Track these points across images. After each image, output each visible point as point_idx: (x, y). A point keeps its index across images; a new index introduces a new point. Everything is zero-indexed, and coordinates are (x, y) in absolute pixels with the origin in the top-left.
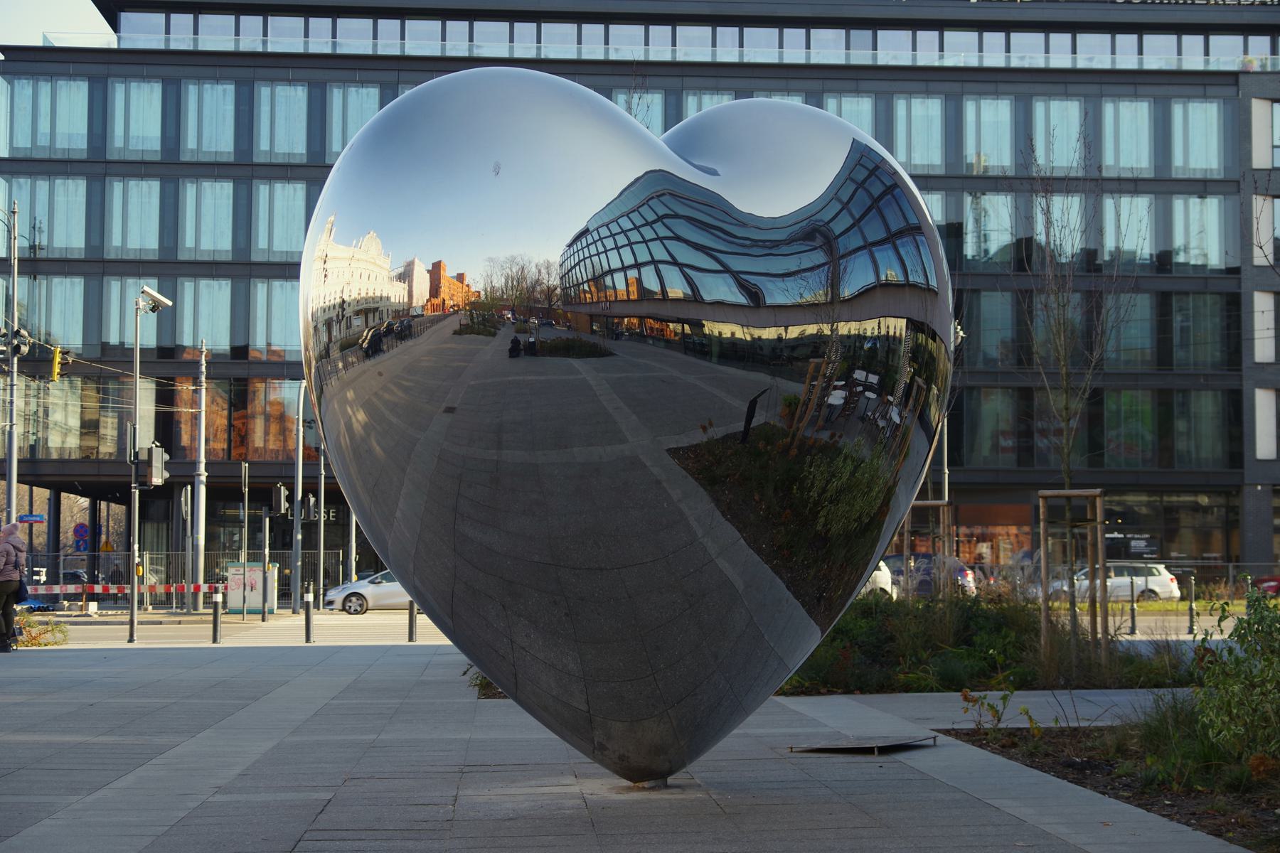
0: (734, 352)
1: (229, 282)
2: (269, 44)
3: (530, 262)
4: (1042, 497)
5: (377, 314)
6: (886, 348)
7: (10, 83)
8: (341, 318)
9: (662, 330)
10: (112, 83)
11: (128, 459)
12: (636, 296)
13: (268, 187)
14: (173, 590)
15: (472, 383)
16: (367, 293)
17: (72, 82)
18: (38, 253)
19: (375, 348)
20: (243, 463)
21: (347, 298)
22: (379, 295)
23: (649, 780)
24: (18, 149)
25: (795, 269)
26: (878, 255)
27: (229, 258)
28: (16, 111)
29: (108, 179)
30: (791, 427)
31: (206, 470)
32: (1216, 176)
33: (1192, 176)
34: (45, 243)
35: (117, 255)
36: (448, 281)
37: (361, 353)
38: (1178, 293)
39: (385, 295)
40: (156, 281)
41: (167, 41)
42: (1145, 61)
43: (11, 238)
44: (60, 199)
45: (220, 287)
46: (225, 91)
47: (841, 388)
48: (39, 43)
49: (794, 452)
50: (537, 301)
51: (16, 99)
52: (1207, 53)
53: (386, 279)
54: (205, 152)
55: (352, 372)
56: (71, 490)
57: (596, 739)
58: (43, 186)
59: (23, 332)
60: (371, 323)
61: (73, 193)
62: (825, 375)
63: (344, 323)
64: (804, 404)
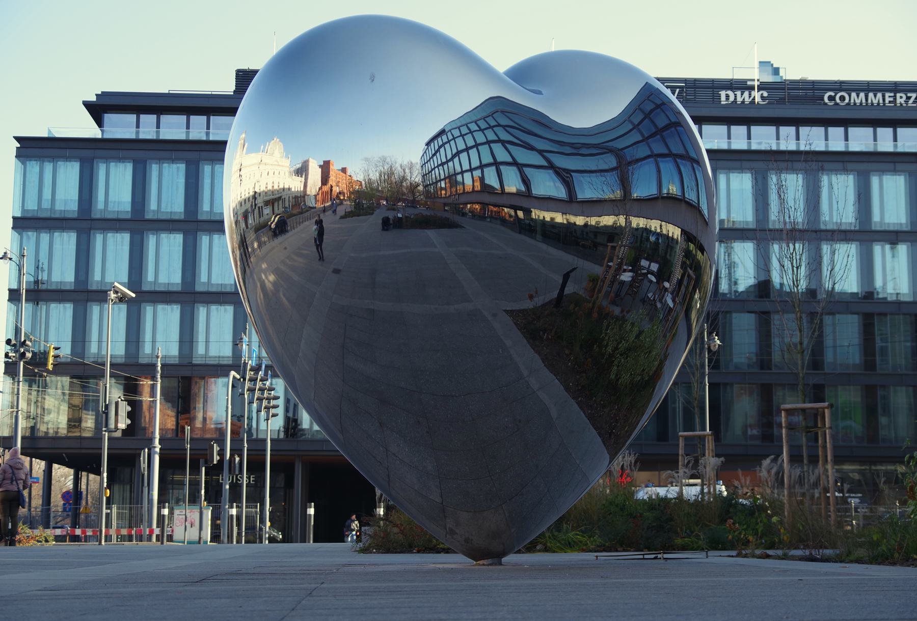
0: (551, 232)
1: (179, 307)
2: (211, 135)
3: (396, 163)
4: (784, 410)
5: (280, 202)
6: (666, 245)
7: (24, 163)
8: (254, 207)
9: (499, 212)
10: (97, 163)
11: (100, 409)
12: (479, 188)
13: (208, 237)
14: (133, 532)
15: (352, 255)
16: (273, 187)
17: (68, 163)
18: (40, 285)
19: (281, 228)
20: (186, 426)
21: (257, 190)
22: (282, 187)
23: (487, 559)
24: (28, 211)
25: (594, 168)
26: (662, 165)
27: (179, 289)
28: (27, 183)
29: (92, 232)
30: (592, 296)
31: (160, 443)
32: (904, 229)
33: (887, 229)
34: (45, 278)
35: (98, 287)
36: (335, 172)
37: (270, 233)
38: (880, 314)
39: (286, 186)
40: (126, 306)
41: (137, 133)
42: (850, 145)
43: (21, 274)
44: (57, 246)
45: (172, 310)
46: (178, 168)
47: (630, 271)
48: (45, 134)
49: (595, 315)
50: (404, 194)
51: (28, 175)
52: (895, 139)
53: (287, 174)
54: (163, 212)
55: (265, 249)
56: (62, 463)
57: (448, 526)
58: (45, 237)
59: (28, 343)
60: (276, 211)
61: (66, 243)
62: (618, 256)
63: (256, 211)
64: (602, 281)
